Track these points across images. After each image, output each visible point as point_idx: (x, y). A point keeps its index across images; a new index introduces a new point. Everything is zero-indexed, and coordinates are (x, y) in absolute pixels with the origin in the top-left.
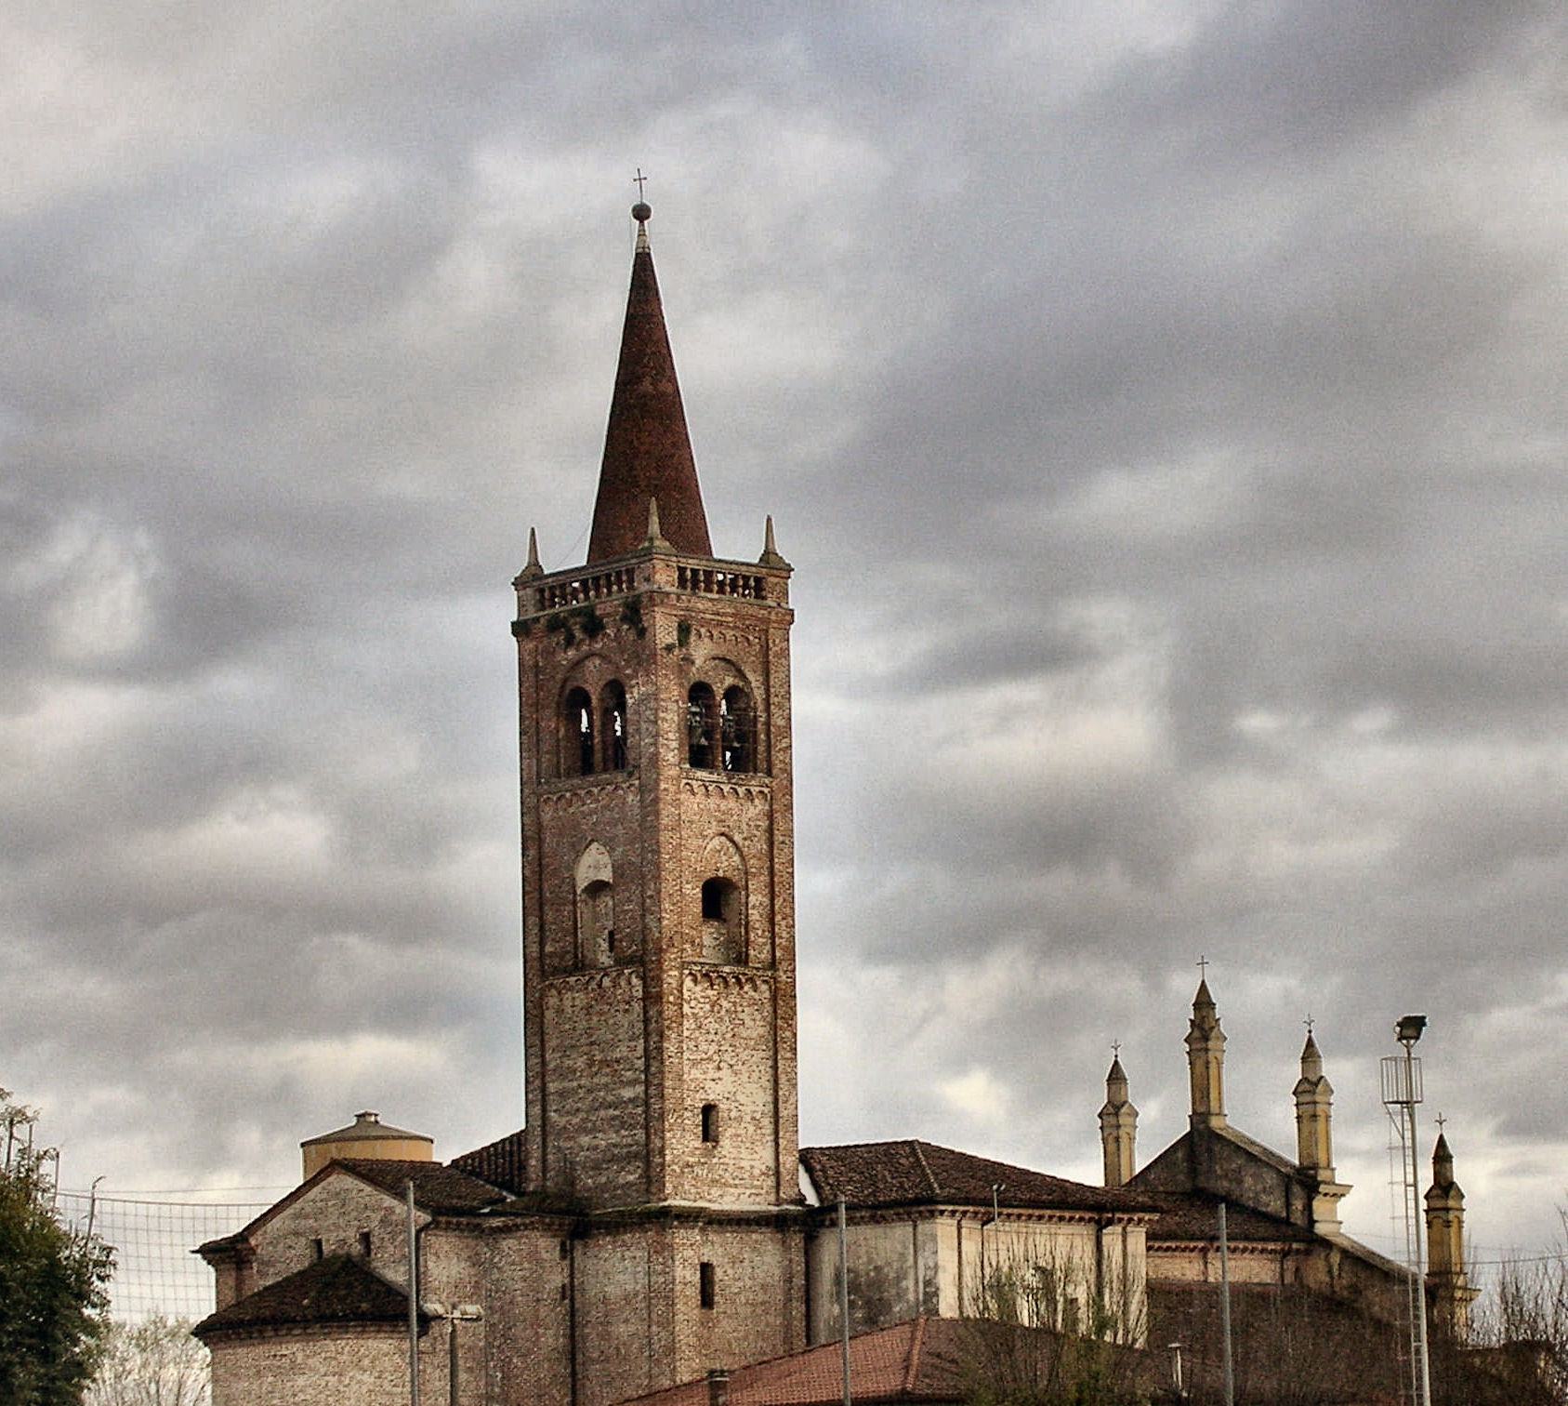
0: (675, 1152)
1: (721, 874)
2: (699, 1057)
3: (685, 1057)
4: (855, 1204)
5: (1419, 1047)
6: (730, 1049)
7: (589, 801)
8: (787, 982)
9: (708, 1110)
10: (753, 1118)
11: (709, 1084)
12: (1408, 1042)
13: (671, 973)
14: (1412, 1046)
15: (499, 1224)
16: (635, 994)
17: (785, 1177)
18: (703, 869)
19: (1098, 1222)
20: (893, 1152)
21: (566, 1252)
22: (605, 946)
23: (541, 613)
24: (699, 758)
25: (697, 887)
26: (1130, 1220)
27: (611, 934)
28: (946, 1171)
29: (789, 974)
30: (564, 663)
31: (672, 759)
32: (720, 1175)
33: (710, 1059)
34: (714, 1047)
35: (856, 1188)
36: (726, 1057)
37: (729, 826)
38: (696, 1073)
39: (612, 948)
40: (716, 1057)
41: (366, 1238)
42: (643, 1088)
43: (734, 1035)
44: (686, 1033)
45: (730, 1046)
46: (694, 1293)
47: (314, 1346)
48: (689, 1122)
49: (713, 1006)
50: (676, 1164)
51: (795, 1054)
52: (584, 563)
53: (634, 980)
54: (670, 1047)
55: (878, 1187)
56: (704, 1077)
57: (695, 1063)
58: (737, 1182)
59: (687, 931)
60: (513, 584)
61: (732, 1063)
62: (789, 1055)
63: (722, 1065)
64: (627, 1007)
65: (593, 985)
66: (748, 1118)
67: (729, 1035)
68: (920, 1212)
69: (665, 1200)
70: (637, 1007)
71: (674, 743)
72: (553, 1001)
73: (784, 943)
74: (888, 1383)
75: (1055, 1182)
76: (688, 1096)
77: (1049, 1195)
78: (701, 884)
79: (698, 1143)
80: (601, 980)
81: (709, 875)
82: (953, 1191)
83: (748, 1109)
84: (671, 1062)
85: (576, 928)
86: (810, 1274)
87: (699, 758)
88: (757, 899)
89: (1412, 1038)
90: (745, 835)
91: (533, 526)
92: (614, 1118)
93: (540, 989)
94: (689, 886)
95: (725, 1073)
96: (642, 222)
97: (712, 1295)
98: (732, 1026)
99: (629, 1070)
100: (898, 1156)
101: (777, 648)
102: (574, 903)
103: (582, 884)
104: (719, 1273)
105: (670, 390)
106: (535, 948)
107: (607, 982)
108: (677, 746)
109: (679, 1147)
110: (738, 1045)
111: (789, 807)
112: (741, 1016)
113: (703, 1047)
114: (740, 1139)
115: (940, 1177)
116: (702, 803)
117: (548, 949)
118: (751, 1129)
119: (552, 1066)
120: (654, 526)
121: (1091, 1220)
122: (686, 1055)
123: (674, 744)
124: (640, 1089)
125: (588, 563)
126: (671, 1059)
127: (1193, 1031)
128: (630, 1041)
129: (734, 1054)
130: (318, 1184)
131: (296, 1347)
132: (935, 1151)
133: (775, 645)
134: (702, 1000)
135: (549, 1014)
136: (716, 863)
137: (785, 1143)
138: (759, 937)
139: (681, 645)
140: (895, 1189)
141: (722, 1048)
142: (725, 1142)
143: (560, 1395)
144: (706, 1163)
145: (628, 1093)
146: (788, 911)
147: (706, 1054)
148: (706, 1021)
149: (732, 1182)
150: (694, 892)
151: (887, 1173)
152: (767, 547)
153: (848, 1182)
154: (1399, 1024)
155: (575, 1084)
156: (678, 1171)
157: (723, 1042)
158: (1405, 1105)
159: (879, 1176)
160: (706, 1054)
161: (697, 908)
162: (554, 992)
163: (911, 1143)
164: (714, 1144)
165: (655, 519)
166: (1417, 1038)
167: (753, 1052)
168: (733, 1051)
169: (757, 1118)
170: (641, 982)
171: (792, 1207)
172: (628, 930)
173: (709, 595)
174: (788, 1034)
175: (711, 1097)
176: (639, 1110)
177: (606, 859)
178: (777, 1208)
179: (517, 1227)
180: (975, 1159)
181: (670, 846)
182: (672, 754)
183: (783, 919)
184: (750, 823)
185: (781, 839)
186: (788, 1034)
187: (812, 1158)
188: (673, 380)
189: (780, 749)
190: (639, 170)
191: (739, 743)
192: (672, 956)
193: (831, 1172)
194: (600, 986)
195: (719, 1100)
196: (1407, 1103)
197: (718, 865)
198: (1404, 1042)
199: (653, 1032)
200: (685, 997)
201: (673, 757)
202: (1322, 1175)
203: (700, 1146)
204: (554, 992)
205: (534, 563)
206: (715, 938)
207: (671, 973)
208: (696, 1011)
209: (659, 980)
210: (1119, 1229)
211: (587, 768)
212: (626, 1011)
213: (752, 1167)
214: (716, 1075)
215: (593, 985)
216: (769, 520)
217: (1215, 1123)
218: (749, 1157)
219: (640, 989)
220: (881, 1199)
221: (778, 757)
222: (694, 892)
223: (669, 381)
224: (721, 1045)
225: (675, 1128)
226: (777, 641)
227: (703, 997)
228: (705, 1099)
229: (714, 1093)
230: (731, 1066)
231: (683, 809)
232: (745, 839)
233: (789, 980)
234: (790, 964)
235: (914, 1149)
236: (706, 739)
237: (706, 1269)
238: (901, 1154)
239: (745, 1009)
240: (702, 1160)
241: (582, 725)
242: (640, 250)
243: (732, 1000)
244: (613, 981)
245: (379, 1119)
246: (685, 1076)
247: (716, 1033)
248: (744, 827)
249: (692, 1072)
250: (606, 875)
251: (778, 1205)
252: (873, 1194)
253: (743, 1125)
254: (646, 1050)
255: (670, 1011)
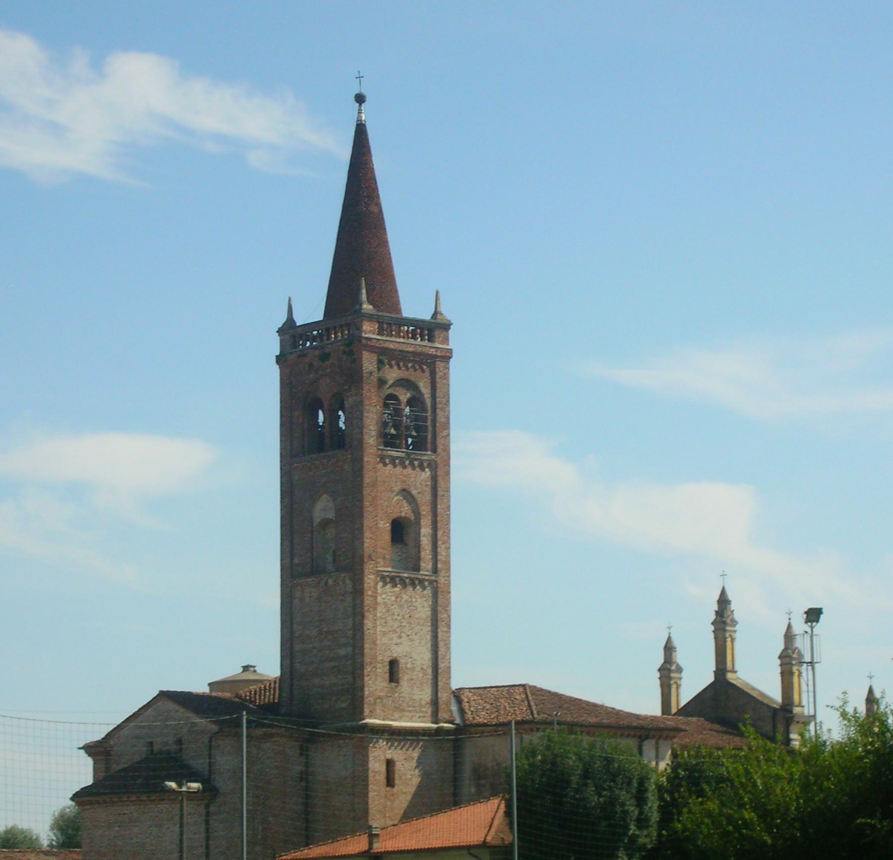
0: (371, 689)
1: (403, 514)
2: (387, 630)
3: (378, 630)
4: (485, 723)
5: (818, 628)
6: (408, 625)
7: (321, 468)
8: (445, 584)
9: (393, 664)
10: (422, 669)
11: (394, 647)
12: (812, 624)
13: (370, 577)
14: (814, 627)
15: (261, 733)
16: (348, 590)
17: (442, 706)
18: (391, 511)
19: (640, 737)
20: (512, 691)
21: (303, 751)
22: (330, 559)
23: (294, 350)
24: (389, 441)
25: (387, 523)
26: (660, 737)
27: (334, 552)
28: (543, 704)
29: (446, 578)
30: (307, 381)
31: (372, 442)
32: (400, 704)
33: (395, 631)
34: (397, 624)
35: (487, 713)
36: (406, 630)
37: (408, 485)
38: (385, 640)
39: (334, 560)
40: (398, 630)
41: (179, 742)
42: (352, 649)
43: (410, 616)
44: (379, 615)
45: (408, 623)
46: (382, 777)
47: (144, 808)
48: (380, 671)
49: (397, 598)
50: (371, 697)
51: (450, 628)
52: (321, 318)
53: (348, 581)
54: (368, 624)
55: (500, 713)
56: (389, 642)
57: (384, 634)
58: (411, 709)
59: (381, 551)
60: (277, 332)
61: (408, 633)
62: (445, 629)
63: (403, 635)
64: (343, 598)
65: (322, 584)
66: (418, 669)
67: (407, 616)
68: (525, 729)
69: (364, 719)
70: (349, 598)
71: (374, 432)
72: (298, 594)
73: (443, 559)
74: (475, 838)
75: (614, 712)
76: (380, 654)
77: (608, 720)
78: (390, 521)
79: (386, 684)
80: (327, 580)
81: (395, 516)
82: (546, 716)
83: (419, 663)
84: (369, 633)
85: (312, 548)
86: (457, 765)
87: (389, 441)
88: (426, 531)
89: (814, 621)
90: (419, 491)
91: (290, 296)
92: (334, 667)
93: (291, 586)
94: (382, 522)
95: (404, 639)
96: (360, 105)
97: (393, 779)
98: (409, 611)
99: (344, 637)
100: (515, 694)
101: (441, 373)
102: (312, 532)
103: (317, 520)
104: (398, 766)
105: (376, 211)
106: (288, 560)
107: (330, 582)
108: (375, 434)
109: (373, 686)
110: (413, 622)
111: (448, 473)
112: (415, 604)
113: (390, 623)
114: (413, 681)
115: (539, 707)
116: (391, 470)
117: (296, 561)
118: (421, 675)
119: (297, 634)
120: (364, 296)
121: (634, 736)
122: (379, 628)
123: (374, 433)
124: (350, 649)
125: (324, 318)
126: (369, 631)
127: (717, 617)
128: (344, 619)
129: (410, 628)
130: (151, 707)
131: (132, 808)
132: (538, 691)
133: (441, 372)
134: (390, 594)
135: (296, 602)
136: (400, 508)
137: (442, 684)
138: (426, 554)
139: (379, 370)
140: (510, 714)
141: (403, 624)
142: (404, 683)
143: (176, 855)
144: (391, 697)
145: (342, 652)
146: (445, 538)
147: (392, 627)
148: (393, 607)
149: (407, 709)
150: (385, 526)
151: (506, 704)
152: (436, 309)
153: (483, 709)
154: (806, 613)
155: (311, 646)
156: (373, 701)
157: (403, 621)
158: (809, 664)
159: (502, 707)
160: (392, 627)
161: (387, 537)
162: (299, 588)
163: (524, 686)
164: (396, 684)
165: (364, 291)
166: (817, 621)
167: (422, 627)
168: (409, 626)
169: (425, 668)
170: (351, 582)
171: (446, 725)
172: (344, 549)
173: (398, 340)
174: (445, 616)
175: (395, 655)
176: (349, 662)
177: (331, 504)
178: (436, 726)
179: (272, 735)
180: (564, 697)
181: (370, 497)
182: (372, 439)
183: (443, 543)
184: (423, 483)
185: (443, 493)
186: (445, 616)
187: (463, 694)
188: (378, 205)
189: (442, 437)
190: (359, 72)
191: (416, 432)
192: (371, 566)
193: (473, 703)
194: (326, 584)
195: (400, 657)
196: (810, 663)
197: (402, 509)
198: (809, 624)
199: (357, 614)
200: (379, 592)
201: (373, 441)
202: (796, 710)
203: (386, 686)
204: (299, 588)
205: (290, 321)
206: (399, 556)
207: (370, 577)
208: (386, 601)
209: (361, 581)
210: (653, 742)
211: (321, 448)
212: (342, 600)
213: (421, 699)
214: (399, 641)
215: (322, 584)
216: (437, 293)
217: (730, 676)
218: (419, 693)
219: (350, 586)
220: (501, 720)
221: (440, 442)
222: (385, 526)
223: (376, 205)
224: (402, 623)
225: (370, 674)
226: (442, 369)
227: (390, 592)
228: (390, 657)
229: (397, 652)
230: (408, 635)
231: (378, 474)
232: (419, 493)
233: (447, 582)
234: (447, 573)
235: (525, 689)
236: (395, 430)
237: (390, 764)
238: (517, 693)
239: (418, 600)
240: (389, 695)
241: (319, 421)
242: (359, 122)
243: (409, 594)
244: (335, 581)
245: (256, 668)
246: (378, 642)
247: (398, 615)
248: (418, 485)
249: (383, 639)
250: (331, 515)
251: (437, 723)
252: (497, 717)
253: (415, 673)
254: (354, 625)
255: (368, 601)
